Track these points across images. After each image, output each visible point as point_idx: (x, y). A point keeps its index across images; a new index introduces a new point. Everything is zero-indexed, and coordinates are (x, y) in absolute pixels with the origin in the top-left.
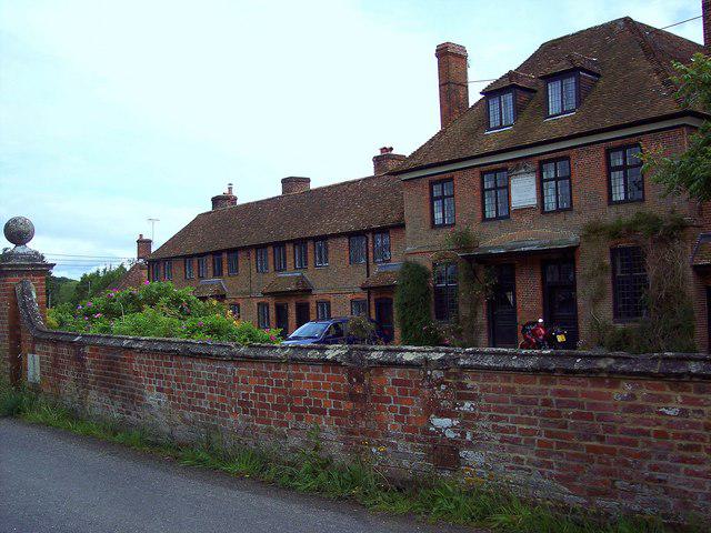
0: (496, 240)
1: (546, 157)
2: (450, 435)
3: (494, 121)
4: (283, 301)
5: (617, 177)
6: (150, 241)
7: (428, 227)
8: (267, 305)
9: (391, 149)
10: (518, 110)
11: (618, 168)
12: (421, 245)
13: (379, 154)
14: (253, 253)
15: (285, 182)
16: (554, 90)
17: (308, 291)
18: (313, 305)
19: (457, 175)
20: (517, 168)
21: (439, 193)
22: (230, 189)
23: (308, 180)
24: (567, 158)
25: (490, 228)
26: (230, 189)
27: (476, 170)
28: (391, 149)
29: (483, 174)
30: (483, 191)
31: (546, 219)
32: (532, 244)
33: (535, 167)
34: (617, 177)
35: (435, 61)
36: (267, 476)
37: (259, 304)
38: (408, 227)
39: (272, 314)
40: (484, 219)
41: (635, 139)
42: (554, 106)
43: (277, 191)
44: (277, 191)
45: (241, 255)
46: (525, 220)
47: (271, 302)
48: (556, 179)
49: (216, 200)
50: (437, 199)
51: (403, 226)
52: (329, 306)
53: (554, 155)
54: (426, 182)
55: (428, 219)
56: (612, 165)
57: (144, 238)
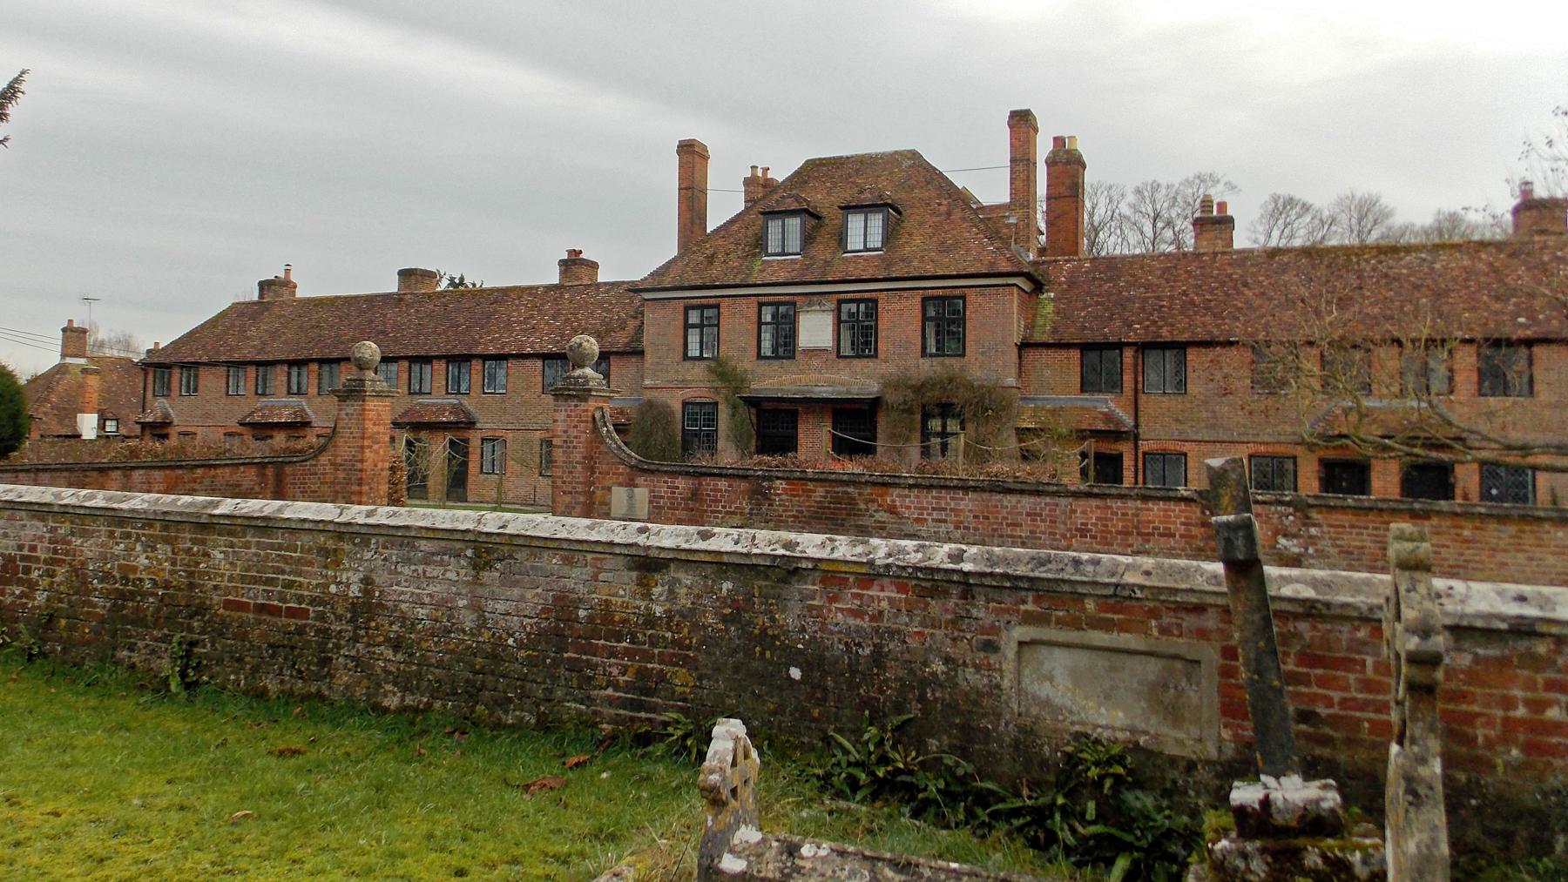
0: (776, 381)
1: (694, 302)
2: (1296, 550)
3: (773, 244)
5: (694, 338)
6: (84, 331)
10: (808, 239)
11: (694, 326)
12: (671, 379)
15: (405, 274)
16: (855, 223)
19: (725, 303)
20: (810, 305)
22: (287, 271)
24: (717, 306)
25: (764, 367)
26: (287, 271)
29: (761, 305)
30: (760, 323)
31: (842, 363)
32: (824, 392)
33: (833, 306)
34: (694, 338)
35: (675, 159)
38: (648, 356)
40: (686, 357)
41: (874, 295)
42: (855, 241)
43: (392, 286)
44: (392, 286)
46: (815, 362)
48: (701, 326)
49: (264, 286)
50: (694, 326)
51: (641, 353)
53: (858, 296)
54: (682, 303)
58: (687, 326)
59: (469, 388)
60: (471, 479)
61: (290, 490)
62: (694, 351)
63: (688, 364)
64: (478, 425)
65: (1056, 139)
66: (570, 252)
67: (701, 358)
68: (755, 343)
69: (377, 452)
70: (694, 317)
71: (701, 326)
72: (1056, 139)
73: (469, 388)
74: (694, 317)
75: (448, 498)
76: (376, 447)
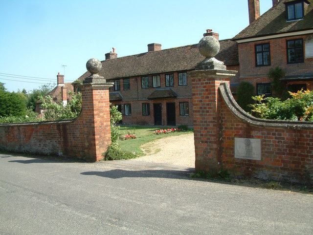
4: (159, 102)
7: (254, 65)
8: (148, 104)
9: (212, 30)
13: (206, 32)
14: (139, 79)
17: (175, 97)
18: (177, 104)
21: (261, 50)
23: (160, 45)
24: (269, 43)
27: (283, 39)
28: (212, 30)
34: (259, 56)
36: (233, 176)
37: (143, 104)
38: (241, 66)
39: (152, 108)
40: (257, 66)
43: (146, 50)
44: (146, 50)
45: (132, 81)
47: (151, 103)
48: (262, 52)
50: (259, 52)
51: (238, 65)
52: (130, 107)
55: (254, 63)
56: (257, 51)
57: (60, 74)
58: (256, 53)
59: (174, 84)
60: (177, 117)
61: (180, 120)
62: (259, 62)
63: (258, 68)
64: (178, 97)
65: (149, 45)
66: (207, 31)
67: (263, 65)
68: (254, 60)
69: (103, 117)
70: (259, 49)
71: (262, 52)
72: (149, 45)
73: (174, 84)
74: (259, 49)
75: (155, 124)
76: (101, 114)
